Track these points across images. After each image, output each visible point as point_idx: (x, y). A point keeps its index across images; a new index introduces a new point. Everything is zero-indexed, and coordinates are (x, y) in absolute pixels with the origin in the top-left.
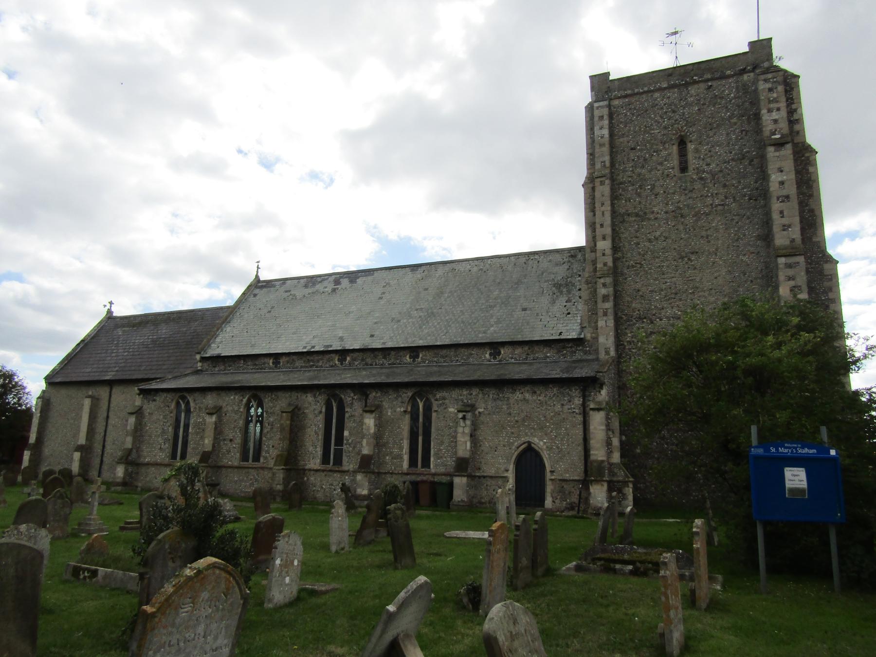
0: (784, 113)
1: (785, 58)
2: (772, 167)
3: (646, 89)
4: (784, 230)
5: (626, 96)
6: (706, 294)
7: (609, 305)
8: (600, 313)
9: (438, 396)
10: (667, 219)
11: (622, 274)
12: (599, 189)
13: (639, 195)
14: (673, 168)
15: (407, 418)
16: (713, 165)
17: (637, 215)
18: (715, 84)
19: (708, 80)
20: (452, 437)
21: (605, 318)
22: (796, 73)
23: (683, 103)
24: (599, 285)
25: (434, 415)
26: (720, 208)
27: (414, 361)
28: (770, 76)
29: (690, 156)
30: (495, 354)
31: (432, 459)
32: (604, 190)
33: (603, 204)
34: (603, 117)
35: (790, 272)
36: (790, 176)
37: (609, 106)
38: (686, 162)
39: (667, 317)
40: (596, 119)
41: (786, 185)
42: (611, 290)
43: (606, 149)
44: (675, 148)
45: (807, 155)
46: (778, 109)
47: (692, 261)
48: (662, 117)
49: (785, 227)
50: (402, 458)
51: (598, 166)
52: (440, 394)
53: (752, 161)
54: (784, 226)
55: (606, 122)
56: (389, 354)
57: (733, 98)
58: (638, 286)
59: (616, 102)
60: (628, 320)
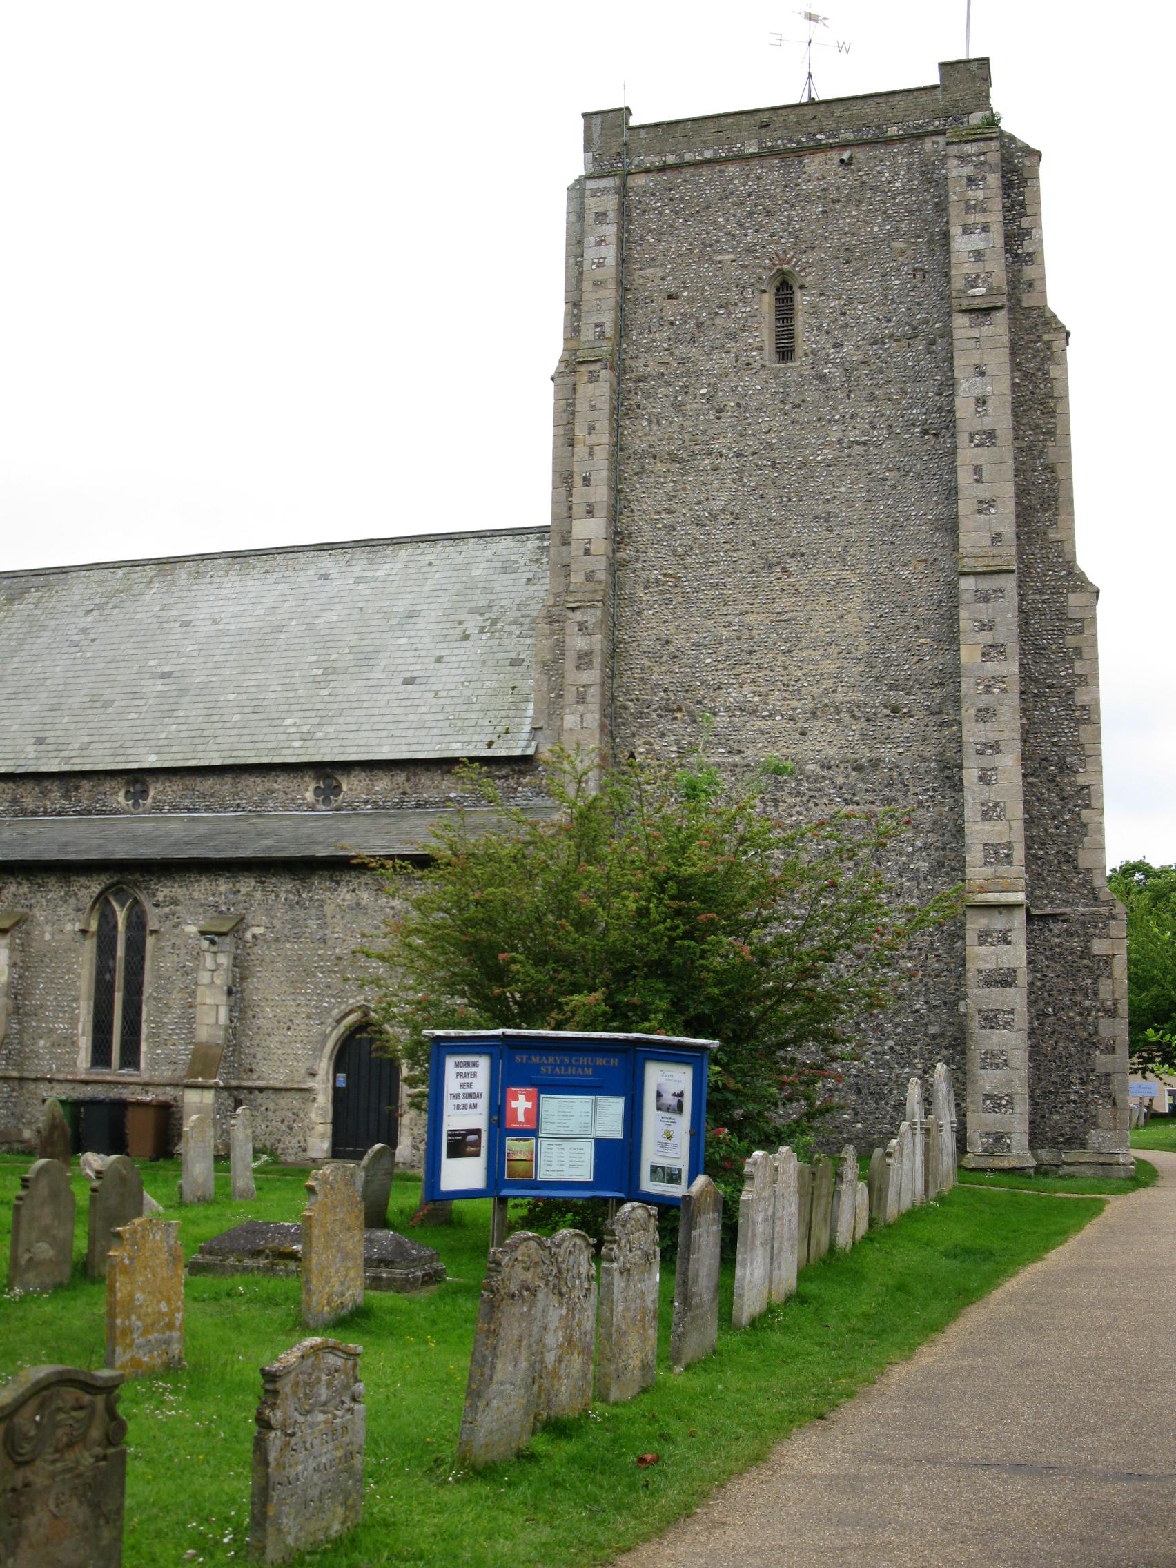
0: (996, 237)
1: (1015, 108)
2: (963, 363)
3: (708, 154)
4: (980, 512)
5: (664, 168)
6: (816, 655)
7: (592, 676)
8: (570, 695)
9: (160, 897)
10: (740, 472)
11: (632, 601)
12: (586, 390)
13: (678, 407)
14: (760, 348)
15: (90, 946)
16: (848, 348)
17: (674, 459)
18: (860, 154)
19: (843, 146)
20: (190, 994)
21: (580, 708)
22: (1033, 145)
23: (790, 194)
24: (572, 628)
25: (150, 941)
26: (858, 449)
27: (136, 804)
28: (971, 149)
29: (801, 323)
30: (329, 792)
31: (144, 1048)
32: (597, 393)
33: (591, 428)
34: (604, 214)
35: (985, 611)
36: (999, 388)
37: (623, 190)
38: (791, 336)
39: (727, 709)
40: (590, 219)
41: (990, 408)
42: (597, 641)
43: (609, 293)
44: (767, 302)
45: (1046, 337)
46: (985, 228)
47: (790, 575)
48: (741, 224)
49: (985, 505)
50: (74, 1044)
51: (588, 334)
52: (166, 891)
53: (933, 342)
54: (980, 502)
55: (610, 230)
56: (77, 788)
57: (901, 192)
58: (666, 631)
59: (641, 181)
60: (641, 715)
